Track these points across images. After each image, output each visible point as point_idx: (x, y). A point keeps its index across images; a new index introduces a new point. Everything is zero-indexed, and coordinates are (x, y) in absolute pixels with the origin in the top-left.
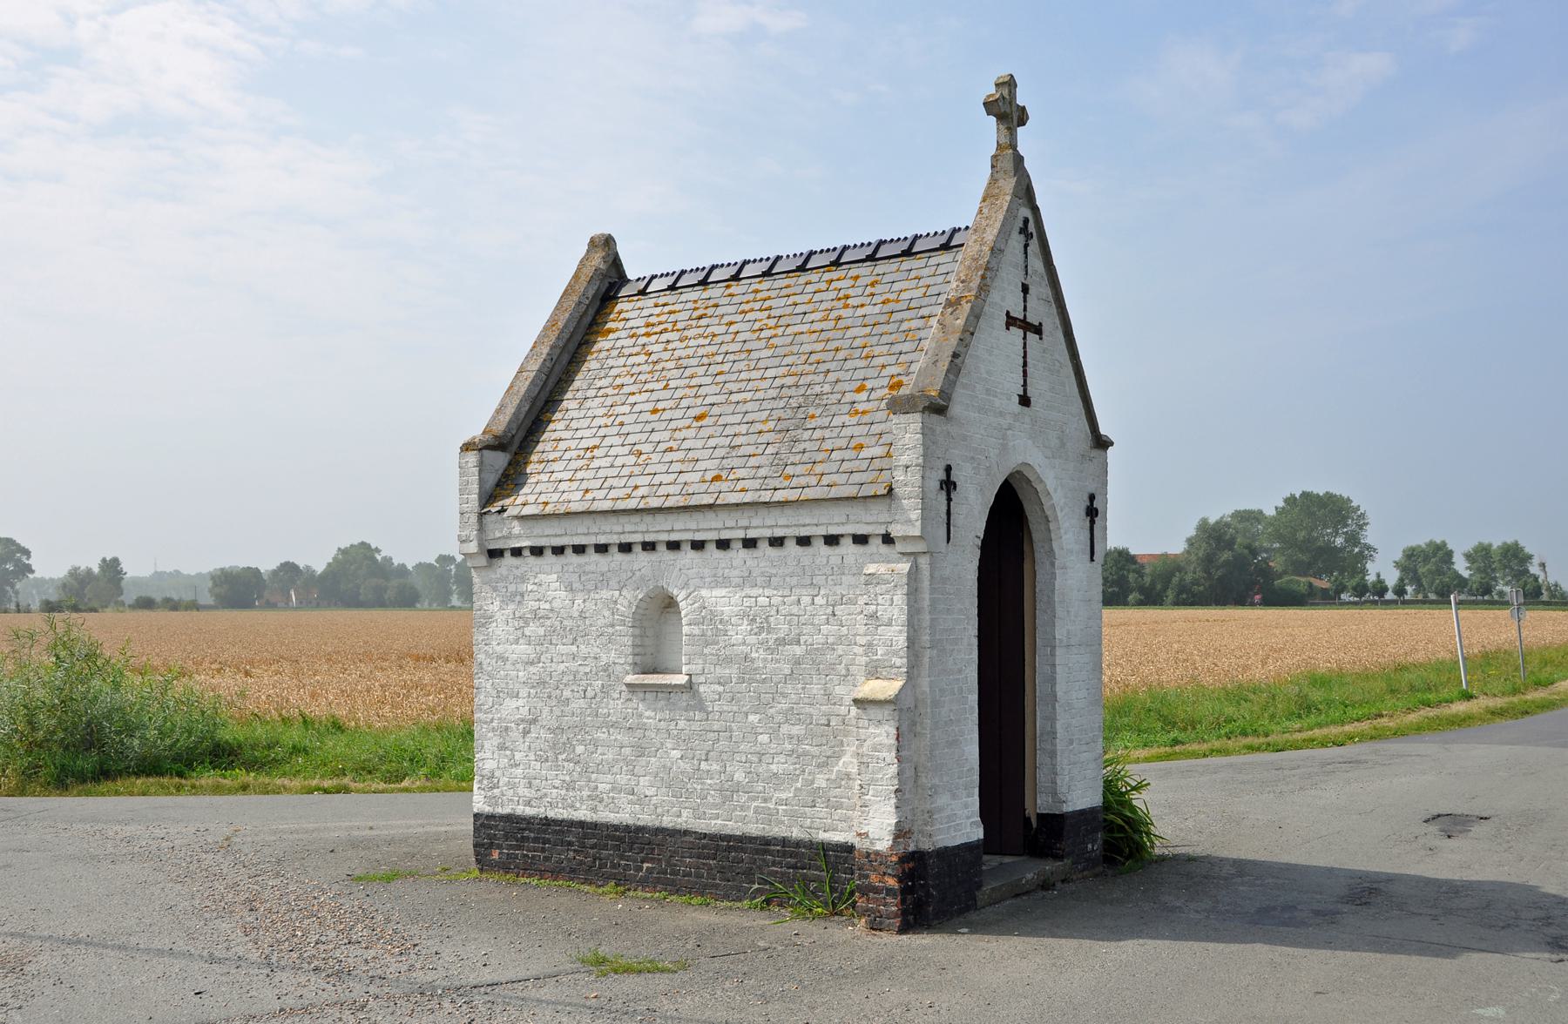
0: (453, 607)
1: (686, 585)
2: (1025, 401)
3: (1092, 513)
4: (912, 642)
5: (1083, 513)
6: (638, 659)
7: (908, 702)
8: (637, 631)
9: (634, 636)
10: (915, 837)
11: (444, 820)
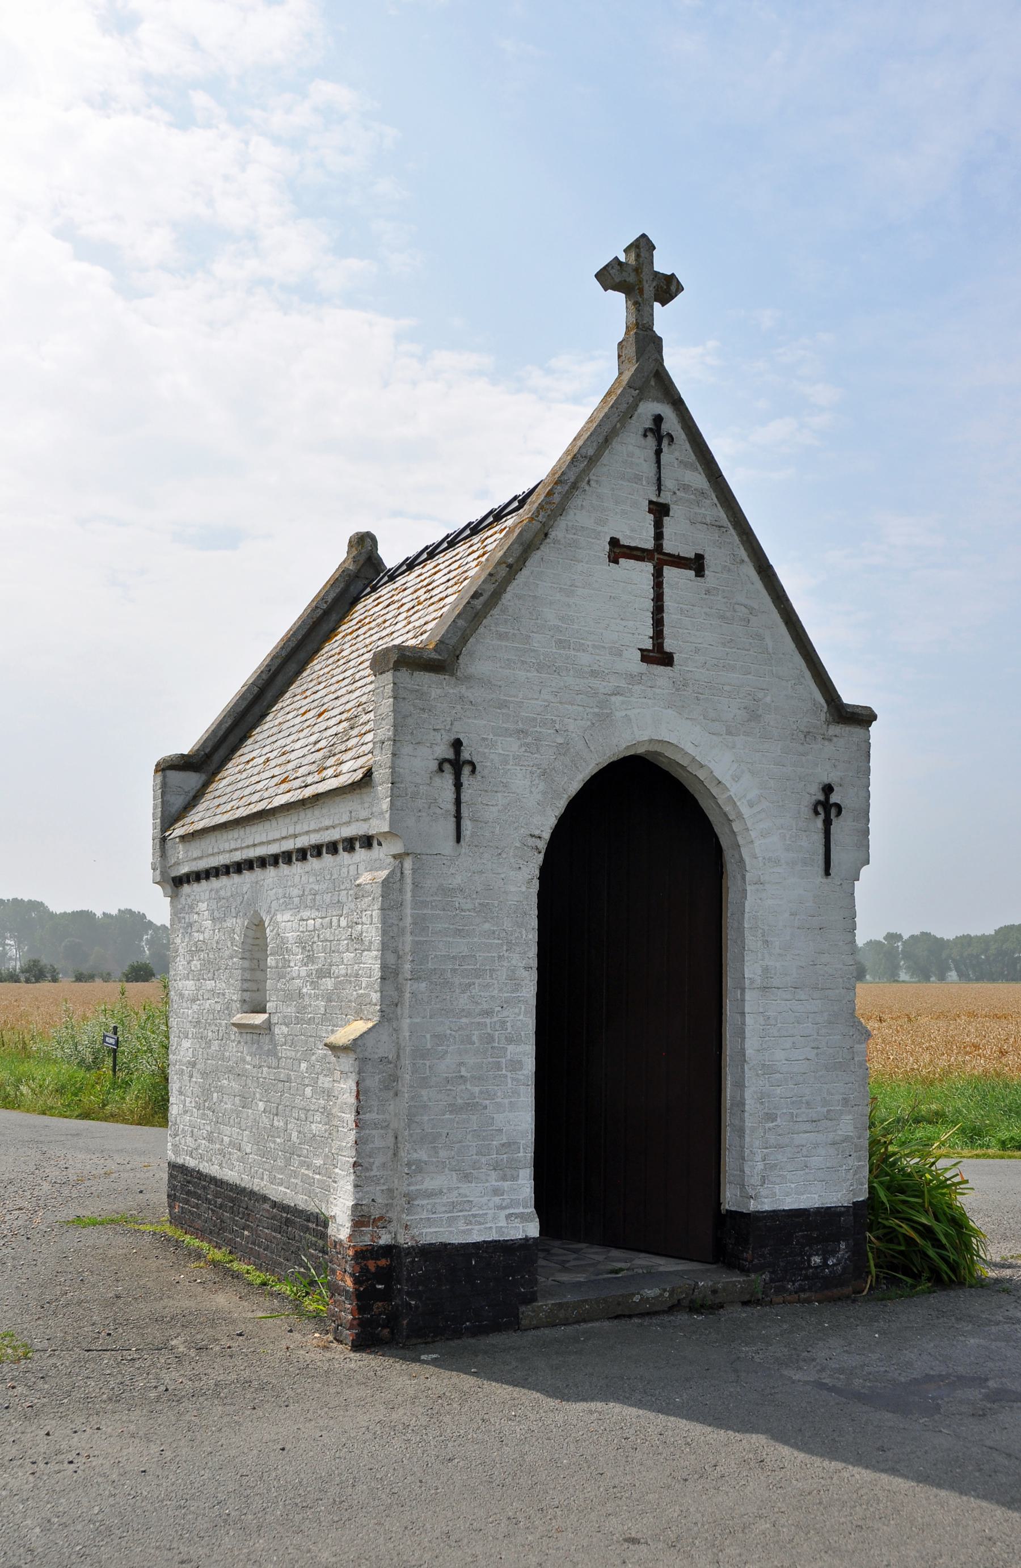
0: (903, 982)
1: (269, 912)
4: (389, 974)
5: (806, 811)
6: (247, 996)
7: (384, 1048)
8: (246, 964)
9: (244, 969)
10: (392, 1227)
11: (132, 1162)
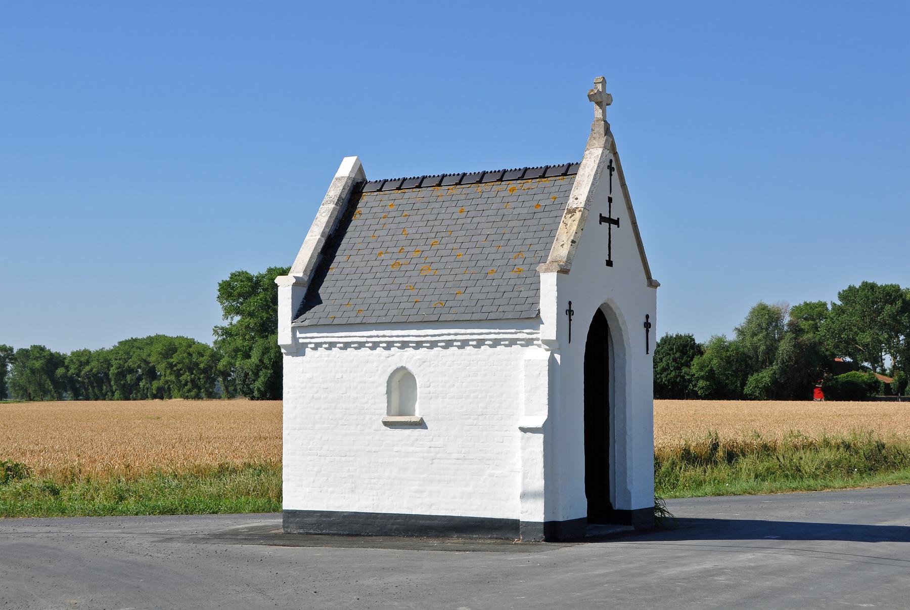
2: (609, 263)
3: (647, 325)
